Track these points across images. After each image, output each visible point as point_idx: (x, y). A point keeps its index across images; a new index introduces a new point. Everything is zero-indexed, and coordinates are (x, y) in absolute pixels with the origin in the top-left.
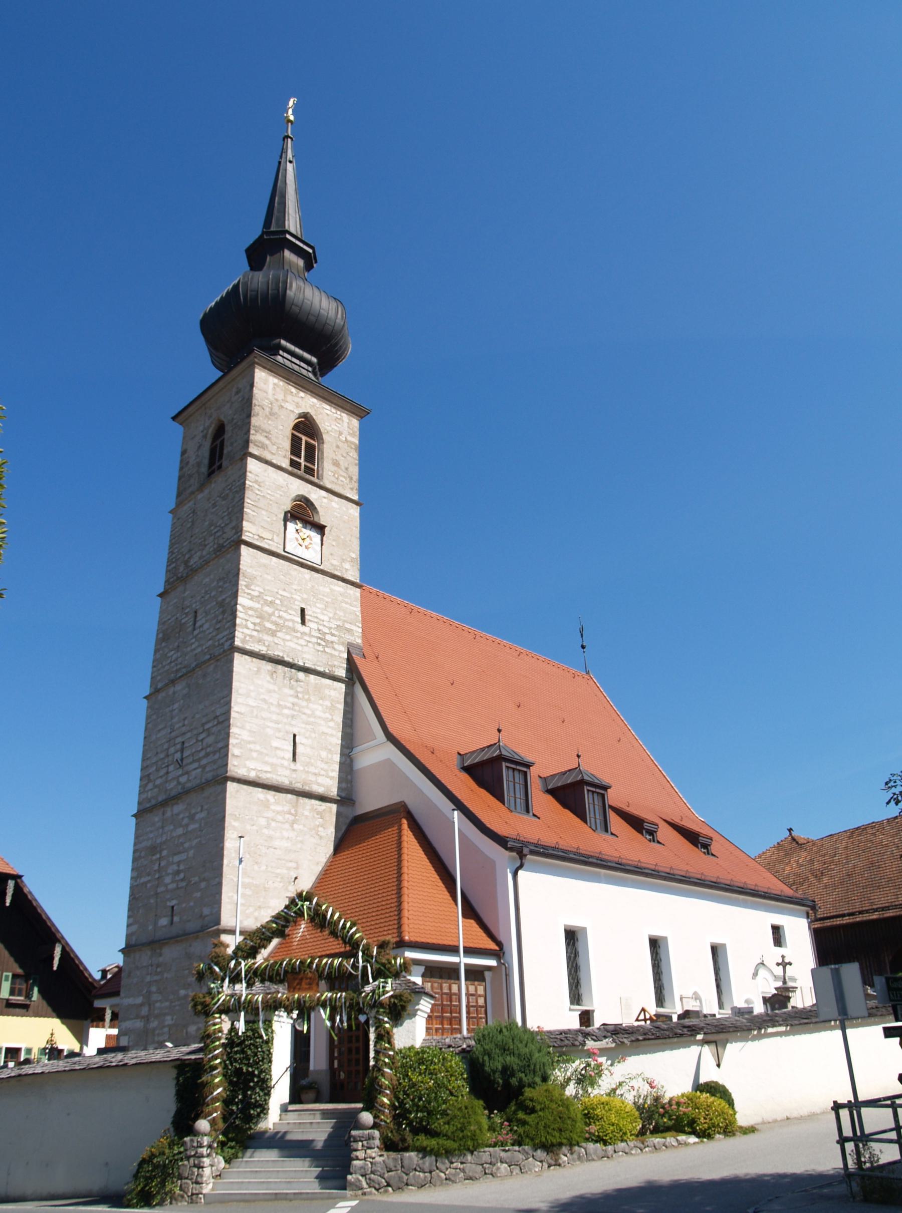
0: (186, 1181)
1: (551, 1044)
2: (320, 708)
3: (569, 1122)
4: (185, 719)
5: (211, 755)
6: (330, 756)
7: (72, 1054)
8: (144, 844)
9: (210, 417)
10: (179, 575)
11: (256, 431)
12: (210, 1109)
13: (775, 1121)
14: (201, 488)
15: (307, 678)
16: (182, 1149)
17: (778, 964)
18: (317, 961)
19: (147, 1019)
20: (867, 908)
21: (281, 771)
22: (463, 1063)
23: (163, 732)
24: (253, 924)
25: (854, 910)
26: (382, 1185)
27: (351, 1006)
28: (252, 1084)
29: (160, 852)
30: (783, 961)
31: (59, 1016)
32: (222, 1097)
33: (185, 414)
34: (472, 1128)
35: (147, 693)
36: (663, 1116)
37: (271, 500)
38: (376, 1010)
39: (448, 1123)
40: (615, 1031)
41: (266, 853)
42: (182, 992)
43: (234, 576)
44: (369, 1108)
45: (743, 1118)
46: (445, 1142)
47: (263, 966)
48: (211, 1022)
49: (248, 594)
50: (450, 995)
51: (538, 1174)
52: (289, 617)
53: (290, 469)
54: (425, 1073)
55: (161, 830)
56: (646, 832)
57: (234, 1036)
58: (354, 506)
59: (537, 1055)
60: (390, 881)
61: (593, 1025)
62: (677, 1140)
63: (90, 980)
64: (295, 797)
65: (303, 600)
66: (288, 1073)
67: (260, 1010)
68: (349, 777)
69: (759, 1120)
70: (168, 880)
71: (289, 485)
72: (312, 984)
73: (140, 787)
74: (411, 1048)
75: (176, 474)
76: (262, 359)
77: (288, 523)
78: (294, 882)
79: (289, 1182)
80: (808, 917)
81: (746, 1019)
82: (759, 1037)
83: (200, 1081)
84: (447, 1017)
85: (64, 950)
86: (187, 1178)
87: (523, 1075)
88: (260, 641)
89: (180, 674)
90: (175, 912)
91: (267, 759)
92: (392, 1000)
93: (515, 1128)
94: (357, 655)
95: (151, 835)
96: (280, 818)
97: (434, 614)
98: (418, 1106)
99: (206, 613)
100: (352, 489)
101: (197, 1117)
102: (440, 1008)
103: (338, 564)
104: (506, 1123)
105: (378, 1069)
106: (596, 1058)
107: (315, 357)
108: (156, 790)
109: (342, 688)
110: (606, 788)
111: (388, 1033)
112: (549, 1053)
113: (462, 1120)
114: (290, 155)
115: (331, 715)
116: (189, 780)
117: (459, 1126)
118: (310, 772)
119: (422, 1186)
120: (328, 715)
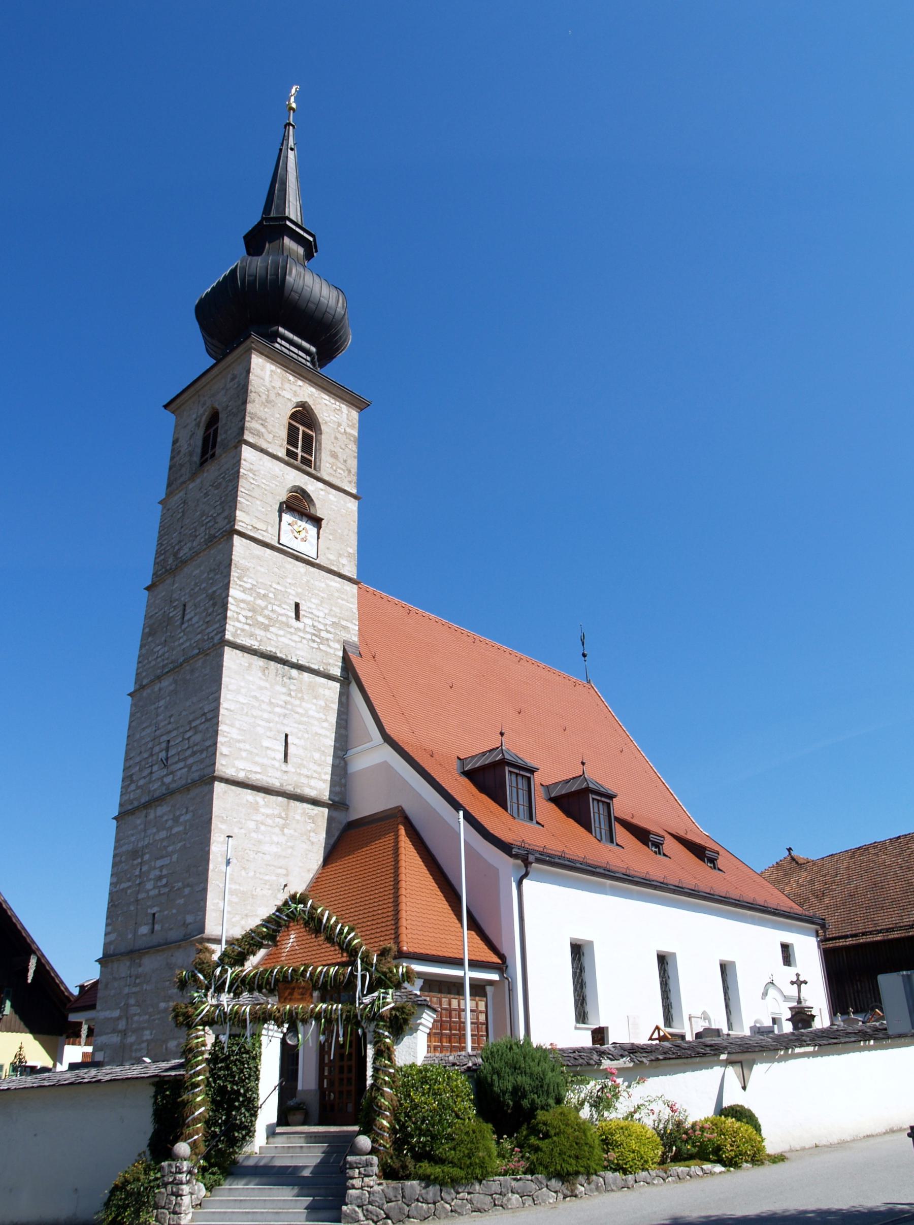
0: (162, 1210)
1: (565, 1063)
2: (314, 707)
3: (586, 1148)
4: (170, 717)
6: (323, 758)
7: (45, 1070)
8: (124, 849)
9: (204, 404)
10: (168, 567)
11: (252, 419)
12: (191, 1131)
13: (804, 1149)
15: (301, 676)
16: (159, 1175)
18: (310, 969)
19: (124, 1033)
20: (871, 929)
21: (271, 772)
22: (469, 1083)
23: (148, 731)
24: (238, 932)
25: (857, 932)
26: (380, 1217)
28: (237, 1104)
30: (798, 979)
31: (32, 1032)
32: (204, 1117)
33: (178, 401)
34: (481, 1154)
35: (132, 690)
36: (686, 1142)
38: (375, 1023)
39: (454, 1149)
40: (633, 1050)
41: (254, 858)
42: (163, 1005)
45: (772, 1143)
46: (451, 1170)
47: (252, 974)
48: (194, 1035)
49: (240, 586)
50: (450, 1011)
52: (283, 612)
53: (286, 458)
54: (428, 1093)
55: (143, 834)
56: (653, 845)
57: (219, 1050)
59: (550, 1074)
60: (386, 889)
61: (608, 1044)
62: (702, 1168)
63: (66, 994)
64: (286, 799)
65: (297, 594)
67: (248, 1022)
70: (149, 886)
71: (285, 476)
72: (305, 995)
74: (412, 1066)
75: (167, 463)
76: (259, 344)
77: (284, 515)
78: (284, 889)
79: (277, 1213)
80: (817, 936)
81: (771, 1038)
84: (446, 1034)
85: (39, 962)
86: (163, 1208)
87: (536, 1096)
88: (252, 635)
89: (167, 670)
90: (156, 920)
91: (257, 759)
92: (394, 1013)
94: (354, 653)
95: (133, 839)
96: (269, 821)
97: (432, 616)
98: (420, 1130)
99: (196, 606)
100: (350, 482)
102: (439, 1024)
103: (335, 559)
104: (516, 1149)
105: (376, 1087)
106: (615, 1078)
107: (314, 346)
110: (611, 797)
111: (388, 1049)
113: (469, 1146)
114: (291, 143)
116: (174, 781)
117: (466, 1152)
119: (425, 1219)
120: (322, 715)
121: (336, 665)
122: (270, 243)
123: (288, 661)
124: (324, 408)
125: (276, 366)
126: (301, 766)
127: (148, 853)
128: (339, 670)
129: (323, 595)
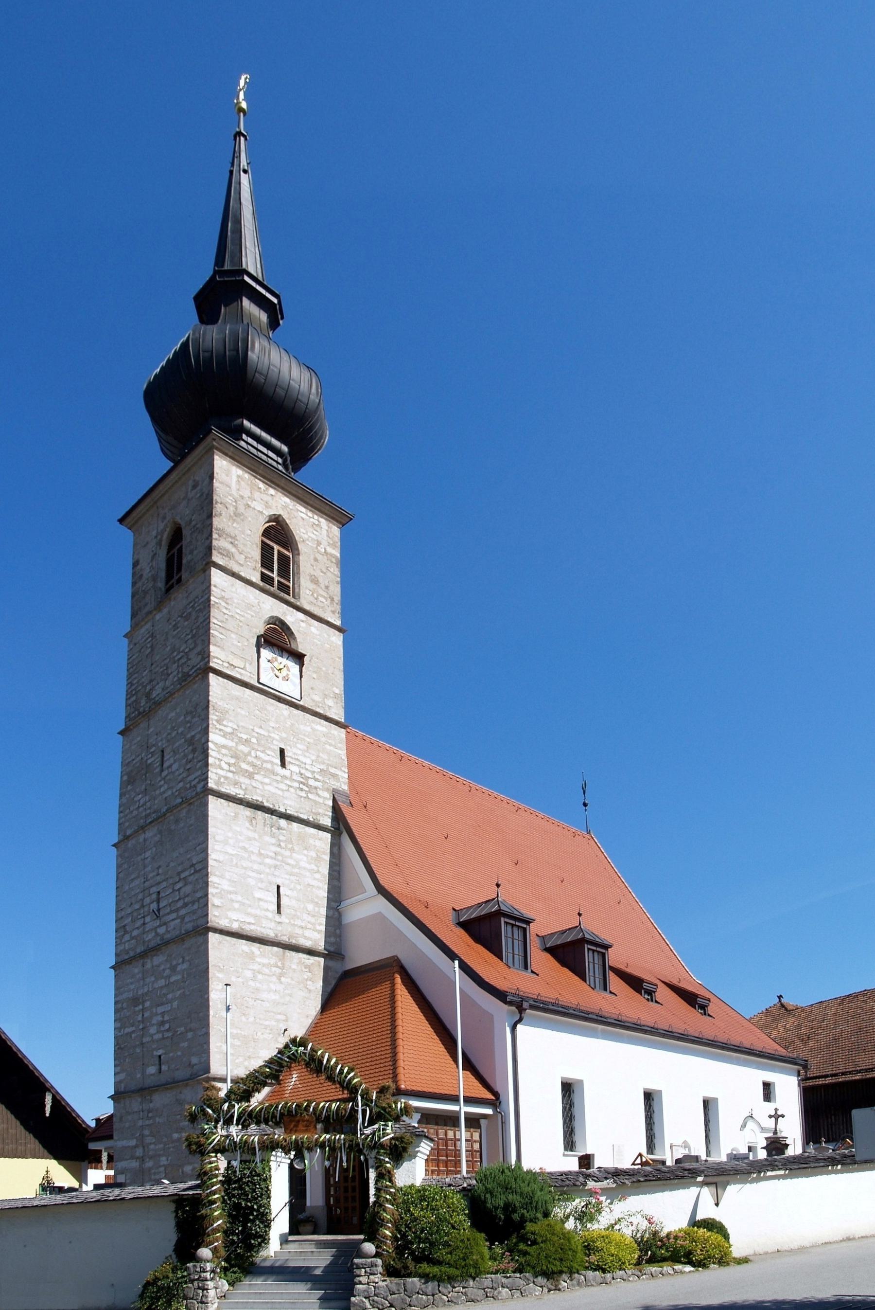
1: (554, 1184)
2: (305, 859)
3: (570, 1253)
4: (158, 868)
5: (190, 905)
6: (317, 909)
7: (71, 1190)
8: (125, 996)
9: (164, 518)
10: (141, 710)
13: (766, 1253)
14: (159, 606)
15: (290, 826)
16: (185, 1274)
17: (770, 1116)
19: (142, 1159)
20: (851, 1070)
21: (265, 923)
22: (464, 1200)
23: (137, 882)
25: (838, 1072)
26: (385, 1306)
27: (350, 1147)
28: (251, 1217)
29: (143, 1003)
31: (55, 1158)
32: (223, 1228)
35: (116, 841)
36: (661, 1247)
37: (241, 621)
38: (376, 1151)
39: (451, 1253)
40: (616, 1174)
42: (176, 1136)
43: (203, 710)
44: (371, 1239)
49: (220, 730)
50: (446, 1141)
51: (539, 1298)
52: (267, 758)
53: (261, 584)
54: (427, 1208)
56: (645, 992)
58: (337, 633)
59: (539, 1193)
63: (83, 1126)
65: (282, 739)
66: (287, 1208)
67: (257, 1150)
68: (338, 932)
69: (752, 1252)
70: (153, 1030)
72: (309, 1126)
73: (116, 938)
74: (412, 1186)
76: (222, 443)
77: (262, 650)
80: (799, 1075)
82: (758, 1180)
83: (199, 1214)
84: (443, 1160)
85: (54, 1098)
86: (192, 1299)
88: (236, 783)
89: (150, 820)
91: (249, 910)
92: (393, 1142)
93: (517, 1258)
94: (343, 802)
95: (132, 987)
96: (266, 971)
97: (426, 763)
98: (420, 1238)
99: (175, 752)
100: (333, 612)
101: (199, 1246)
103: (320, 700)
107: (286, 445)
108: (133, 941)
109: (328, 839)
110: (607, 947)
111: (389, 1172)
112: (550, 1192)
115: (316, 866)
118: (297, 925)
119: (425, 1307)
120: (313, 867)
121: (326, 815)
122: (225, 306)
123: (275, 811)
124: (301, 523)
125: (243, 470)
126: (294, 917)
127: (148, 1000)
128: (330, 820)
129: (308, 740)
